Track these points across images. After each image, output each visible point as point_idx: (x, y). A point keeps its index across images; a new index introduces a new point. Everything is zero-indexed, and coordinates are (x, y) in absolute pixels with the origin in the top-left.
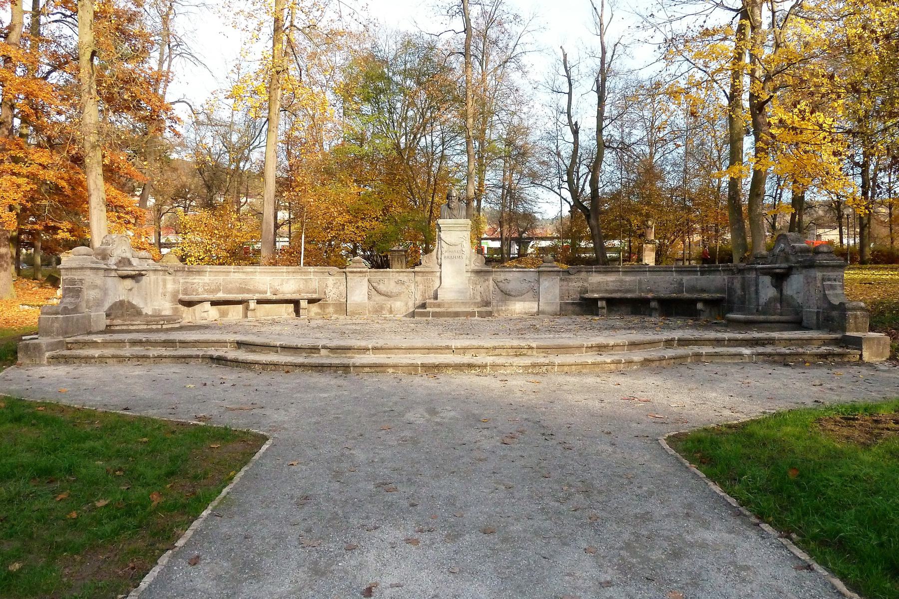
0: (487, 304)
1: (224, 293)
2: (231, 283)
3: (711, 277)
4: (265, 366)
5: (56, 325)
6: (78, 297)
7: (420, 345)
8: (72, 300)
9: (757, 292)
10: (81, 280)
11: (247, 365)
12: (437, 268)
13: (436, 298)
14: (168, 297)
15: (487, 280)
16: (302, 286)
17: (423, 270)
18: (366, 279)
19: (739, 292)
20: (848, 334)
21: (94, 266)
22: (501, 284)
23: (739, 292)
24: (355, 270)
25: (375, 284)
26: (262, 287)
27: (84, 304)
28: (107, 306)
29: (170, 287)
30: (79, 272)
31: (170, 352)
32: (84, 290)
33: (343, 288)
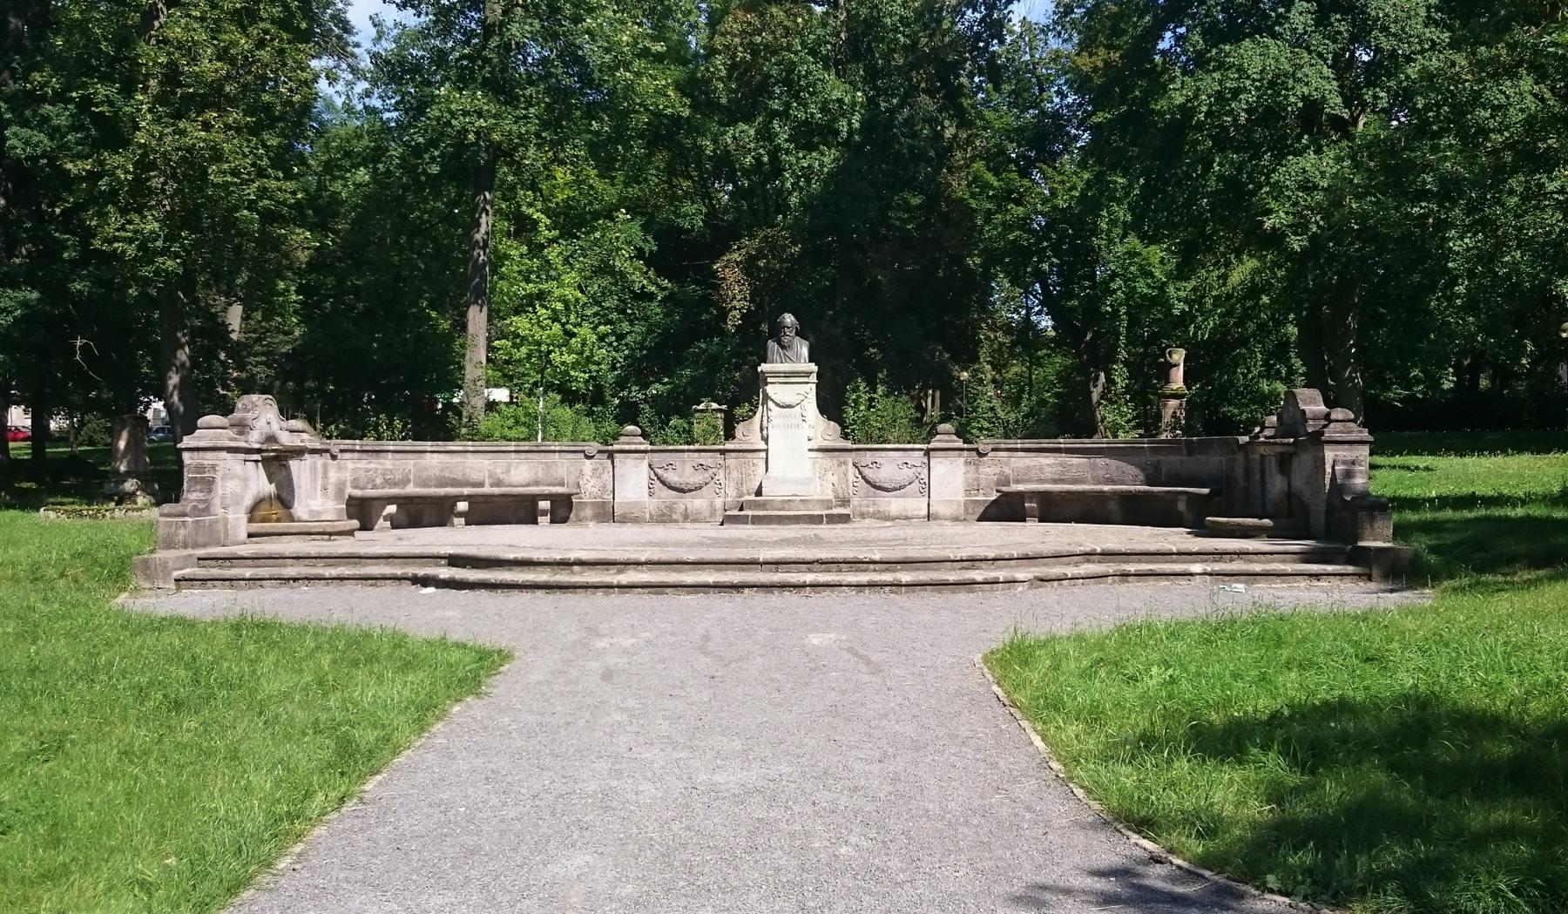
0: (845, 502)
1: (416, 485)
2: (426, 469)
3: (1203, 458)
4: (586, 587)
5: (182, 532)
6: (210, 491)
7: (877, 557)
8: (201, 496)
9: (1263, 482)
10: (214, 467)
11: (970, 584)
12: (762, 446)
13: (759, 493)
14: (331, 490)
15: (845, 463)
16: (540, 474)
17: (738, 447)
18: (646, 463)
19: (1241, 482)
20: (1361, 544)
21: (233, 444)
22: (866, 471)
23: (1241, 482)
24: (627, 447)
25: (660, 472)
26: (475, 476)
27: (217, 501)
28: (248, 501)
29: (333, 476)
30: (209, 454)
31: (1110, 568)
32: (218, 480)
33: (607, 477)
